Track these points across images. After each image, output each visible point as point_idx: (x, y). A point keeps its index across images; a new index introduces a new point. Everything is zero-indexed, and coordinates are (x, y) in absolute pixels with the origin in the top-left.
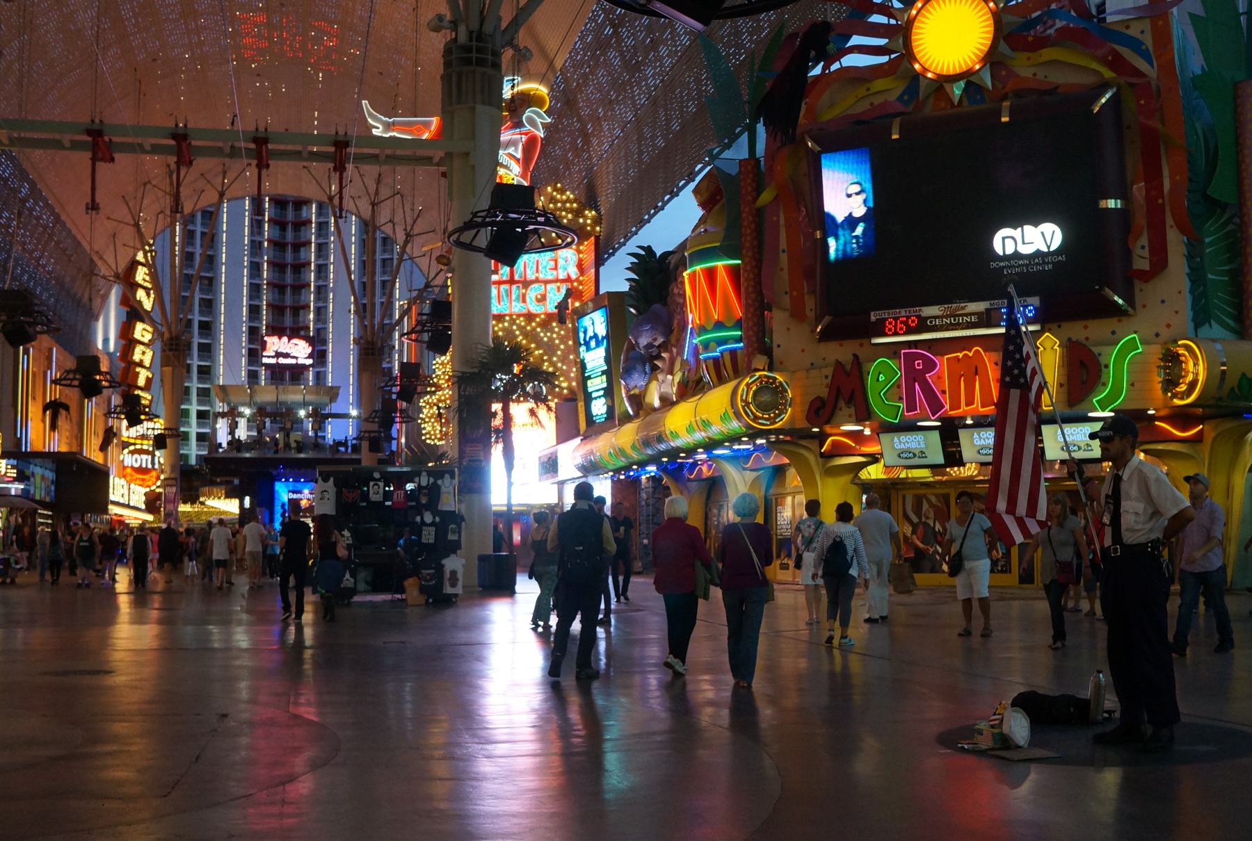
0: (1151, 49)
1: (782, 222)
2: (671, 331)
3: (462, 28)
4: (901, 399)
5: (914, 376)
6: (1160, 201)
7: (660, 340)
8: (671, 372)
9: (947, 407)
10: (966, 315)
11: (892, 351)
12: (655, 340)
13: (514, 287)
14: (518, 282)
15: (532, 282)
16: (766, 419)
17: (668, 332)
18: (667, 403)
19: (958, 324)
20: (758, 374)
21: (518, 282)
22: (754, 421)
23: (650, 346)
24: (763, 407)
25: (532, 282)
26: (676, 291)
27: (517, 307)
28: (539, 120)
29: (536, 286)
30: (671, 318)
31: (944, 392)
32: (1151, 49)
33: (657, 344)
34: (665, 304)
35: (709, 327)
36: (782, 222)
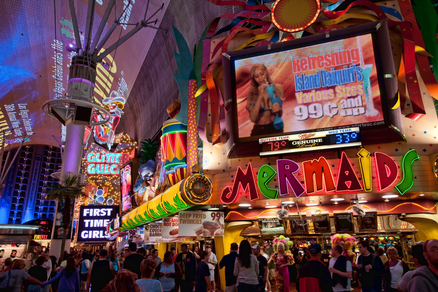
0: (400, 12)
1: (209, 101)
2: (155, 171)
3: (80, 51)
4: (276, 187)
5: (284, 174)
6: (415, 82)
7: (151, 174)
8: (154, 186)
9: (306, 190)
10: (315, 139)
11: (270, 160)
12: (149, 174)
13: (106, 165)
14: (107, 163)
15: (112, 164)
16: (200, 199)
17: (154, 171)
18: (150, 198)
19: (311, 144)
20: (196, 174)
21: (107, 163)
22: (192, 200)
23: (146, 176)
24: (197, 193)
25: (112, 164)
26: (158, 154)
27: (107, 172)
28: (163, 204)
29: (114, 165)
30: (156, 165)
31: (303, 182)
32: (400, 12)
33: (149, 175)
34: (154, 160)
35: (171, 161)
36: (209, 101)
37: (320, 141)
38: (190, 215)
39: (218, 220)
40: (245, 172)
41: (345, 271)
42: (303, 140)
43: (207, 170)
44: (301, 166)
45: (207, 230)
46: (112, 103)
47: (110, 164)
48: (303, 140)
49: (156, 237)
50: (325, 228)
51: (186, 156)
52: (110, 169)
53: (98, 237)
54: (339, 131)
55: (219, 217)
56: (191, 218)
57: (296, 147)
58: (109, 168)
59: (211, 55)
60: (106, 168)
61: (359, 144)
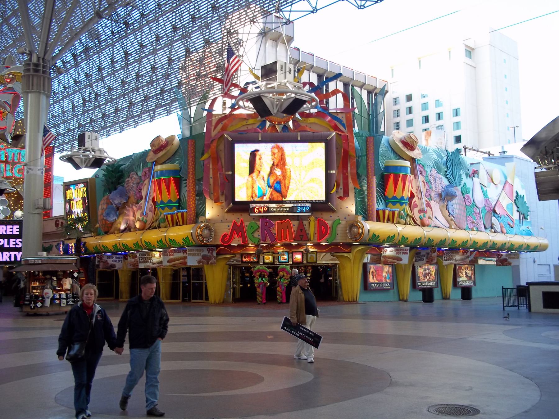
1: (211, 166)
10: (285, 208)
15: (16, 163)
25: (16, 163)
29: (18, 165)
36: (211, 166)
37: (288, 209)
38: (194, 250)
39: (212, 253)
40: (239, 224)
41: (225, 171)
42: (278, 208)
43: (209, 220)
44: (275, 223)
45: (204, 261)
46: (9, 74)
47: (14, 164)
48: (278, 208)
49: (144, 264)
50: (238, 295)
51: (180, 199)
52: (14, 171)
53: (8, 260)
54: (299, 205)
55: (213, 251)
56: (194, 252)
57: (274, 212)
58: (12, 169)
59: (213, 128)
60: (7, 169)
61: (309, 214)
